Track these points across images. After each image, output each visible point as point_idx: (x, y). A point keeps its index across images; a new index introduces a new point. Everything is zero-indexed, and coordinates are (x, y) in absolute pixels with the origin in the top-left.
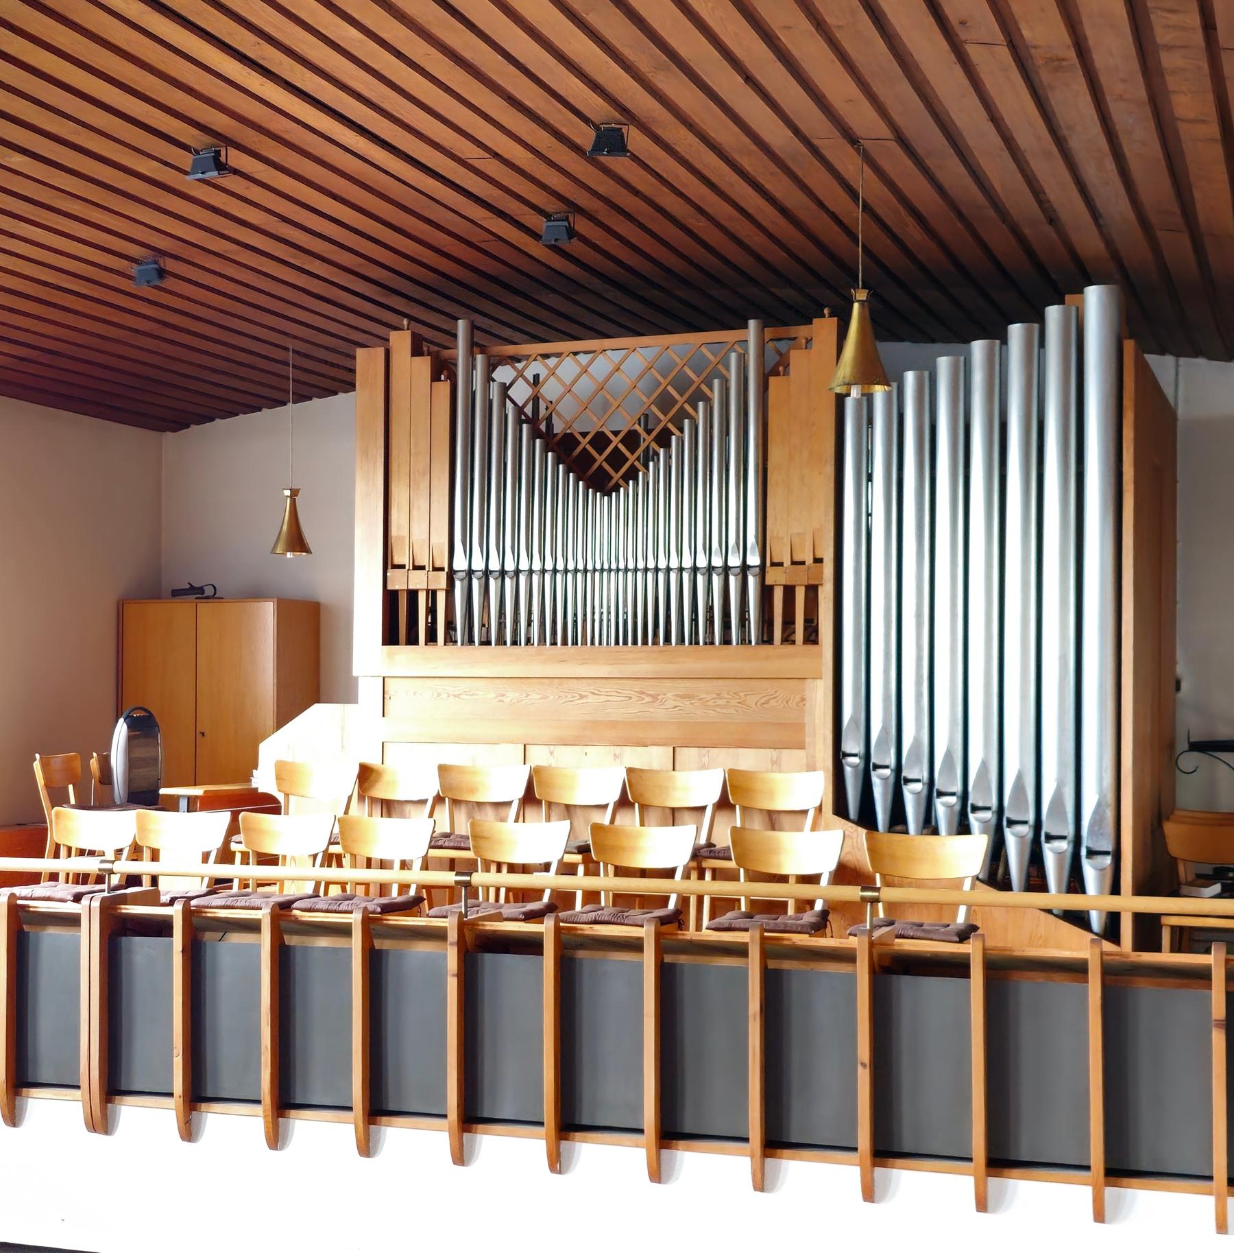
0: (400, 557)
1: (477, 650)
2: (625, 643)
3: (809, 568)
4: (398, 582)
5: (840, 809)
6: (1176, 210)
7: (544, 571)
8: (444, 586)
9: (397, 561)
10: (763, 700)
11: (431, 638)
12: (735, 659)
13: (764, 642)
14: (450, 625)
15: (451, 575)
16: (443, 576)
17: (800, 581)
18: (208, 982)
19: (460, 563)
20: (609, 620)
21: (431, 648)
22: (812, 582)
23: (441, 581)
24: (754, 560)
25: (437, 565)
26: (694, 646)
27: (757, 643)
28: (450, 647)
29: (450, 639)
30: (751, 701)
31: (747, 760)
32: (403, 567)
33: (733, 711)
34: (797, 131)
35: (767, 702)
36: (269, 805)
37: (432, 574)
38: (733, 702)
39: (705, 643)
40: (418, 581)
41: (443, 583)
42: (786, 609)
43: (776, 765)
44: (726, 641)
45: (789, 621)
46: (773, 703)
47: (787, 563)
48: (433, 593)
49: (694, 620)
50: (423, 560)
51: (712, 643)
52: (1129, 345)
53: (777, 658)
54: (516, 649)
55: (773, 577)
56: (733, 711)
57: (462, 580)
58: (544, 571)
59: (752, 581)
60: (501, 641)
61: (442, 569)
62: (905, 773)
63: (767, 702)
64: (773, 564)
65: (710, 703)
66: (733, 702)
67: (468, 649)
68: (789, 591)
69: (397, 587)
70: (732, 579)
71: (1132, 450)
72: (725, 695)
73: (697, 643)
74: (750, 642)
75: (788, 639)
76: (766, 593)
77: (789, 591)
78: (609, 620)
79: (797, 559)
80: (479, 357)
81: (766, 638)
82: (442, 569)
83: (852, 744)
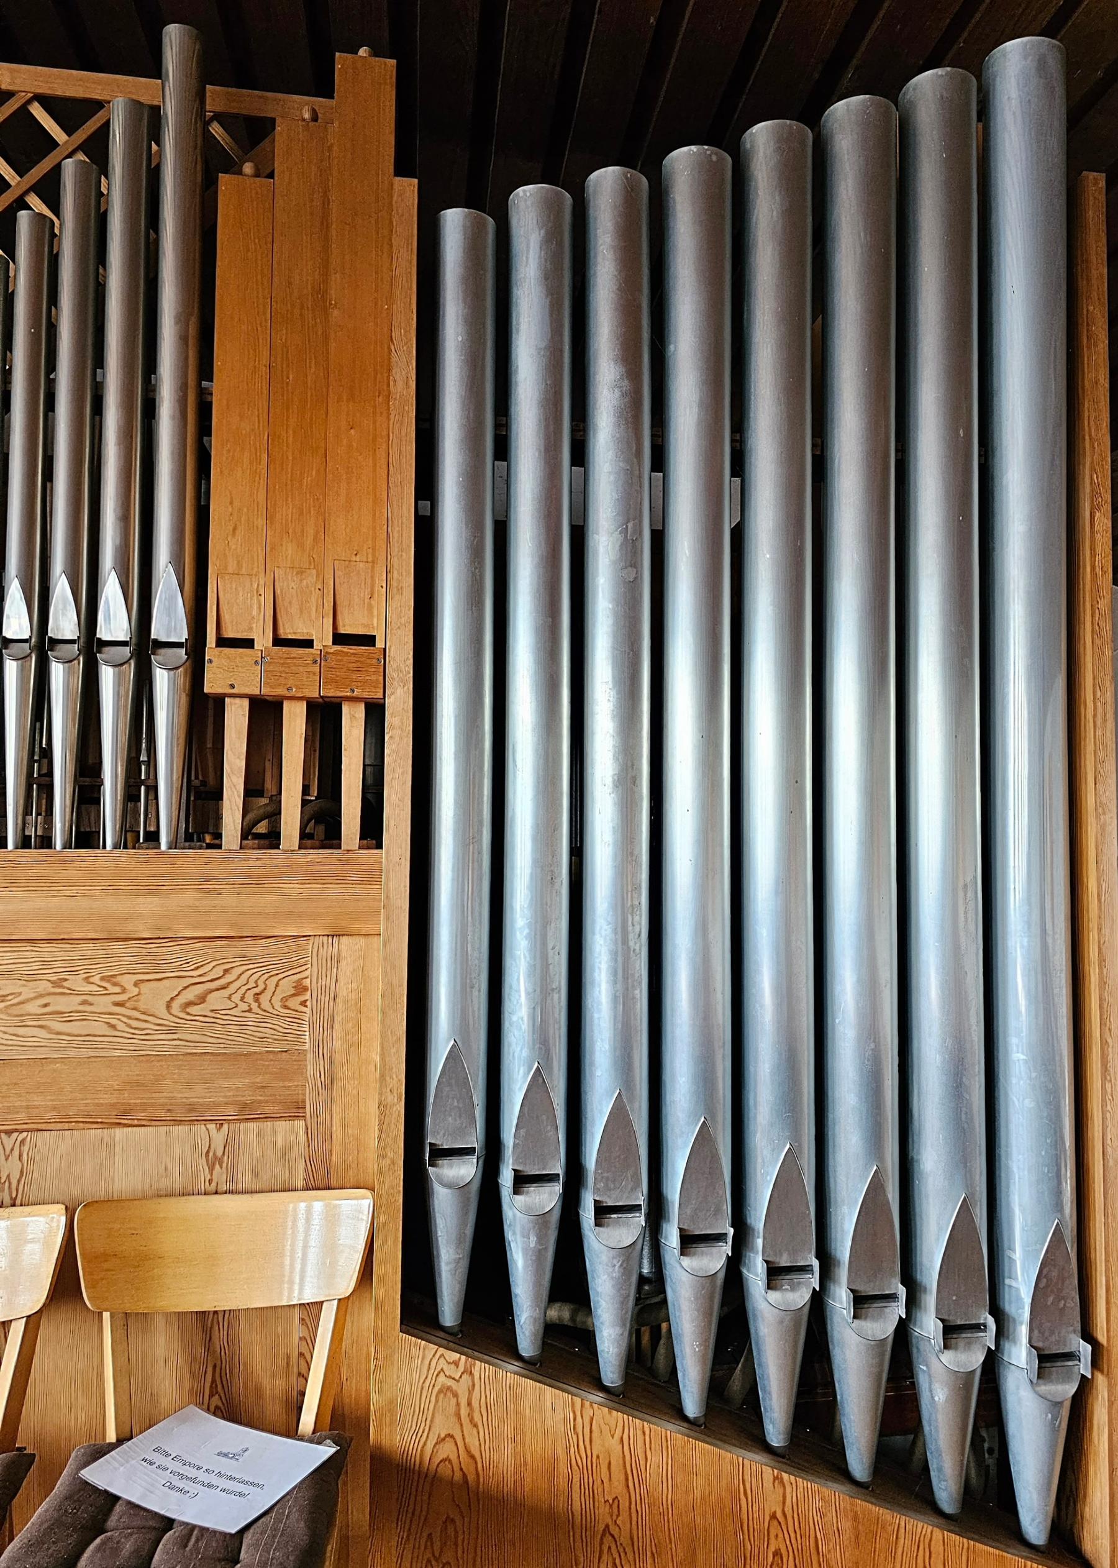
3: (324, 655)
5: (418, 1311)
10: (190, 995)
12: (99, 887)
17: (300, 684)
18: (998, 519)
22: (331, 692)
24: (170, 621)
30: (155, 996)
31: (131, 1158)
33: (101, 1028)
34: (326, 248)
35: (202, 999)
36: (269, 518)
38: (103, 1003)
39: (24, 843)
42: (270, 771)
43: (221, 1178)
44: (86, 837)
45: (260, 785)
46: (216, 1001)
47: (263, 641)
51: (46, 842)
52: (1095, 183)
53: (227, 884)
55: (223, 673)
56: (101, 1028)
59: (164, 685)
62: (436, 1135)
63: (202, 999)
64: (222, 642)
65: (33, 1008)
66: (103, 1003)
68: (265, 714)
72: (76, 983)
75: (200, 824)
76: (203, 713)
77: (265, 714)
81: (200, 824)
83: (452, 1123)
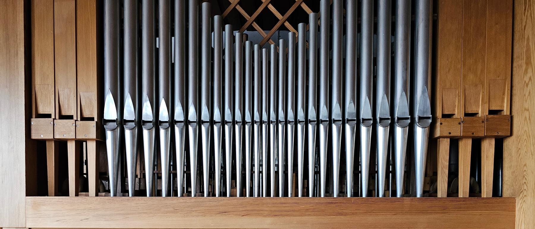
0: (45, 106)
1: (132, 202)
2: (286, 194)
4: (42, 130)
6: (355, 115)
7: (234, 122)
8: (94, 136)
9: (42, 110)
11: (82, 186)
13: (284, 196)
14: (102, 175)
15: (102, 124)
16: (92, 125)
19: (111, 112)
20: (261, 172)
21: (81, 198)
23: (90, 131)
25: (86, 115)
26: (211, 198)
27: (274, 196)
28: (102, 198)
29: (102, 189)
32: (49, 116)
37: (79, 123)
40: (65, 130)
41: (93, 134)
48: (80, 144)
49: (317, 173)
50: (70, 109)
54: (172, 200)
57: (113, 130)
58: (122, 122)
60: (172, 192)
61: (92, 119)
64: (444, 116)
67: (121, 199)
69: (42, 137)
70: (162, 132)
71: (272, 11)
73: (214, 195)
74: (320, 196)
76: (432, 143)
78: (261, 172)
79: (446, 112)
80: (216, 18)
82: (92, 119)
